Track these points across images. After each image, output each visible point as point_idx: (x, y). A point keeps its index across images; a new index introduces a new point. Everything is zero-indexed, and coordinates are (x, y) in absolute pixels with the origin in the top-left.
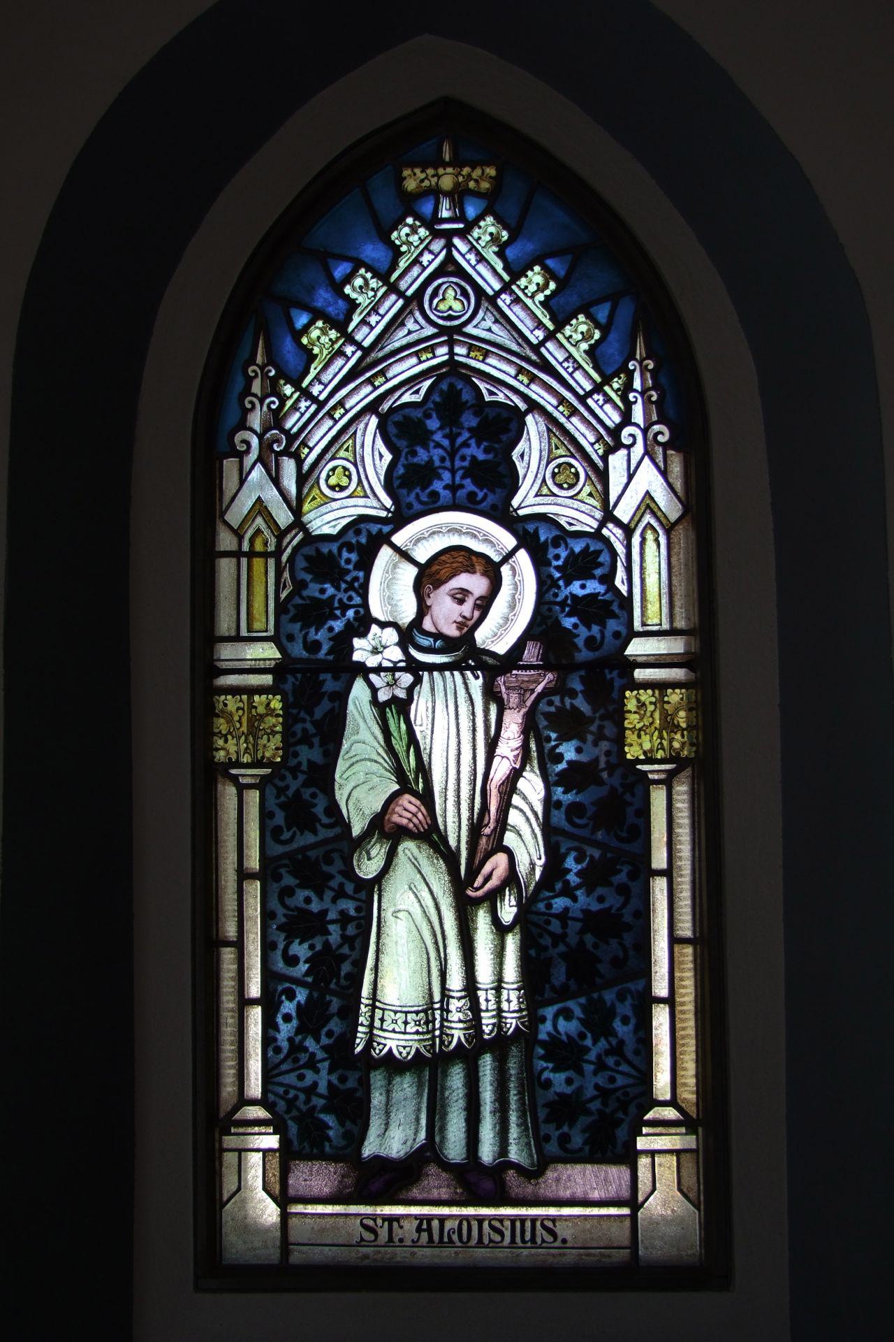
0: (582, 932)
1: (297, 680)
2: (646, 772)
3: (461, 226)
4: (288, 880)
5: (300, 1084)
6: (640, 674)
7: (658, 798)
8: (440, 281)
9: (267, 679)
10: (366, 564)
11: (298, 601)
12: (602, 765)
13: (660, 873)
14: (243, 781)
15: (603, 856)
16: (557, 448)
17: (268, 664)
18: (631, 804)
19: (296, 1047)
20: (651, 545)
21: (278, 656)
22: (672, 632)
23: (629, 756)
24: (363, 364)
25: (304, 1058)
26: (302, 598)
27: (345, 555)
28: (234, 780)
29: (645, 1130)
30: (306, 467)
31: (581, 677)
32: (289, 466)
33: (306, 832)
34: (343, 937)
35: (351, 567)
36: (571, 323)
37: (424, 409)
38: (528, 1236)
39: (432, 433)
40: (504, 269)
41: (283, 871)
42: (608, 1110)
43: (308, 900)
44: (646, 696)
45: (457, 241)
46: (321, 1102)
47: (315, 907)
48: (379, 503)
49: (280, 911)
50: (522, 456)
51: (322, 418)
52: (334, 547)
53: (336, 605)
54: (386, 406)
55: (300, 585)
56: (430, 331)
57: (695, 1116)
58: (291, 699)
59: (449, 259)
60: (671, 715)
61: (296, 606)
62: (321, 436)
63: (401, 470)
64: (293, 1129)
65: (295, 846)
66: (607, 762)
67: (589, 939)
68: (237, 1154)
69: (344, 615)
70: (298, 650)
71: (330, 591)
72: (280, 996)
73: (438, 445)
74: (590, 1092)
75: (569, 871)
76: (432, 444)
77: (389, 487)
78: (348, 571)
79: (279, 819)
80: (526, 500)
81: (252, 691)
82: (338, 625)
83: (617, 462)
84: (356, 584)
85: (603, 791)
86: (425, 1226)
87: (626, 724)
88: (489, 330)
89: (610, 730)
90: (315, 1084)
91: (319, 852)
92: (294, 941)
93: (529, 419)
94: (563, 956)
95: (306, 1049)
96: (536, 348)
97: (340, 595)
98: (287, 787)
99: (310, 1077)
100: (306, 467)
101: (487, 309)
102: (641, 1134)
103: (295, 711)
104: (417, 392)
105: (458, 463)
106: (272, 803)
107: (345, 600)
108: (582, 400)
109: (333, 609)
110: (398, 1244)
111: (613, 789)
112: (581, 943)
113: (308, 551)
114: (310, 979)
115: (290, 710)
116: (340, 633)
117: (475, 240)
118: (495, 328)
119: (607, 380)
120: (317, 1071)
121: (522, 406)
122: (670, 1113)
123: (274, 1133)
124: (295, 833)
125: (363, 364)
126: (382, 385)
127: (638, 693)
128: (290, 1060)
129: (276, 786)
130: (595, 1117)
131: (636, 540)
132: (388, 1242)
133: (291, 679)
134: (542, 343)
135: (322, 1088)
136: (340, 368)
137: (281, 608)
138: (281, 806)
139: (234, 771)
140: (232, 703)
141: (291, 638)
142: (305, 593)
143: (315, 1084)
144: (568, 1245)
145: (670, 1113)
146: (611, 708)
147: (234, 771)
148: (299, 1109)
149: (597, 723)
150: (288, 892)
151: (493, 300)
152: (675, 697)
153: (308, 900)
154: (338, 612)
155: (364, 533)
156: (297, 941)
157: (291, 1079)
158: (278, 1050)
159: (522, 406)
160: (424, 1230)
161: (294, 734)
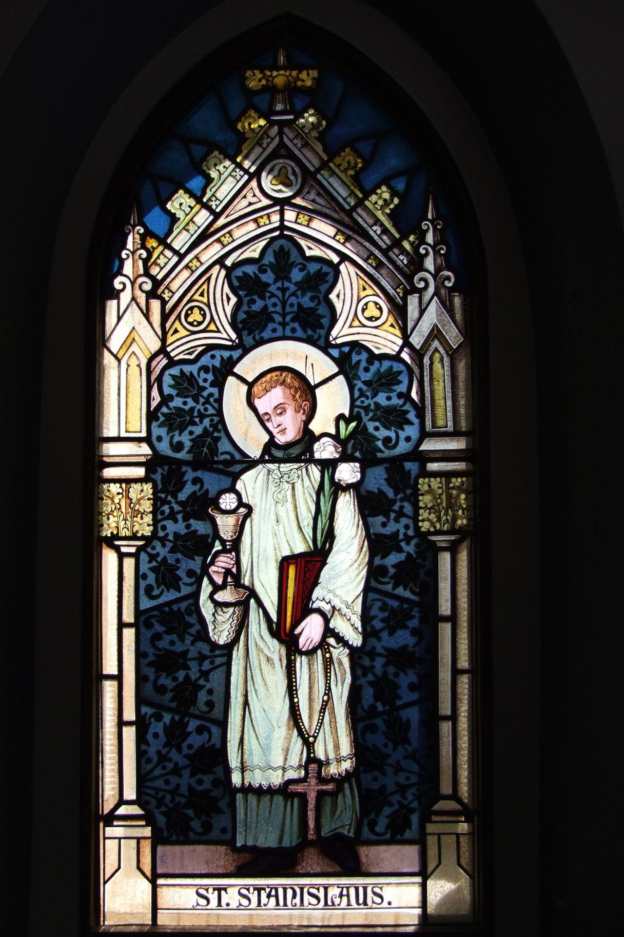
0: (385, 665)
1: (164, 471)
2: (435, 541)
3: (292, 117)
4: (159, 628)
5: (167, 787)
6: (433, 466)
7: (445, 559)
8: (275, 162)
9: (140, 472)
10: (220, 384)
11: (165, 410)
12: (401, 536)
13: (445, 619)
14: (124, 550)
15: (400, 606)
16: (364, 289)
17: (143, 459)
18: (423, 566)
19: (162, 758)
20: (437, 366)
21: (150, 452)
22: (456, 434)
23: (423, 529)
24: (212, 229)
25: (170, 766)
26: (168, 407)
27: (203, 375)
28: (117, 549)
29: (434, 818)
30: (169, 306)
31: (386, 468)
32: (156, 305)
33: (171, 590)
34: (200, 671)
35: (207, 385)
36: (377, 191)
37: (259, 265)
38: (361, 900)
39: (269, 285)
40: (324, 150)
41: (153, 621)
42: (405, 802)
43: (172, 643)
44: (435, 483)
45: (286, 130)
46: (183, 800)
47: (179, 647)
48: (227, 334)
49: (151, 651)
50: (338, 296)
51: (181, 270)
52: (193, 369)
53: (196, 414)
54: (229, 262)
55: (166, 399)
56: (266, 202)
57: (472, 808)
58: (160, 486)
59: (281, 144)
60: (455, 498)
61: (164, 415)
62: (180, 282)
63: (241, 316)
64: (162, 820)
65: (161, 600)
66: (405, 534)
67: (391, 670)
68: (118, 840)
69: (201, 422)
70: (164, 447)
71: (191, 403)
72: (149, 719)
73: (273, 295)
74: (391, 787)
75: (374, 617)
76: (268, 295)
77: (233, 325)
78: (205, 388)
79: (151, 578)
80: (341, 333)
81: (129, 481)
82: (198, 430)
83: (413, 302)
84: (212, 400)
85: (402, 557)
86: (273, 893)
87: (421, 504)
88: (314, 201)
89: (408, 508)
90: (178, 786)
91: (183, 605)
92: (161, 675)
93: (342, 268)
94: (371, 684)
95: (170, 760)
96: (349, 213)
97: (200, 407)
98: (158, 554)
99: (174, 779)
100: (169, 306)
101: (312, 185)
102: (431, 822)
103: (163, 496)
104: (255, 251)
105: (288, 309)
106: (145, 567)
107: (202, 411)
108: (385, 252)
109: (192, 417)
110: (264, 907)
111: (409, 554)
112: (385, 673)
113: (175, 371)
114: (174, 705)
115: (159, 495)
116: (199, 436)
117: (270, 213)
118: (319, 200)
119: (405, 237)
120: (180, 776)
121: (336, 259)
122: (452, 805)
123: (146, 825)
124: (163, 590)
125: (212, 229)
126: (229, 243)
127: (429, 481)
128: (160, 767)
129: (148, 553)
130: (397, 807)
131: (426, 360)
132: (328, 887)
133: (160, 470)
134: (354, 208)
135: (184, 790)
136: (195, 231)
137: (151, 416)
138: (152, 569)
139: (117, 543)
140: (114, 488)
141: (160, 439)
142: (172, 405)
143: (178, 786)
144: (392, 906)
145: (452, 805)
146: (408, 492)
147: (117, 543)
148: (166, 806)
149: (398, 504)
150: (157, 637)
151: (313, 175)
152: (456, 482)
153: (172, 643)
154: (197, 420)
155: (218, 358)
156: (164, 674)
157: (160, 783)
158: (149, 761)
159: (336, 259)
160: (273, 896)
161: (163, 513)
